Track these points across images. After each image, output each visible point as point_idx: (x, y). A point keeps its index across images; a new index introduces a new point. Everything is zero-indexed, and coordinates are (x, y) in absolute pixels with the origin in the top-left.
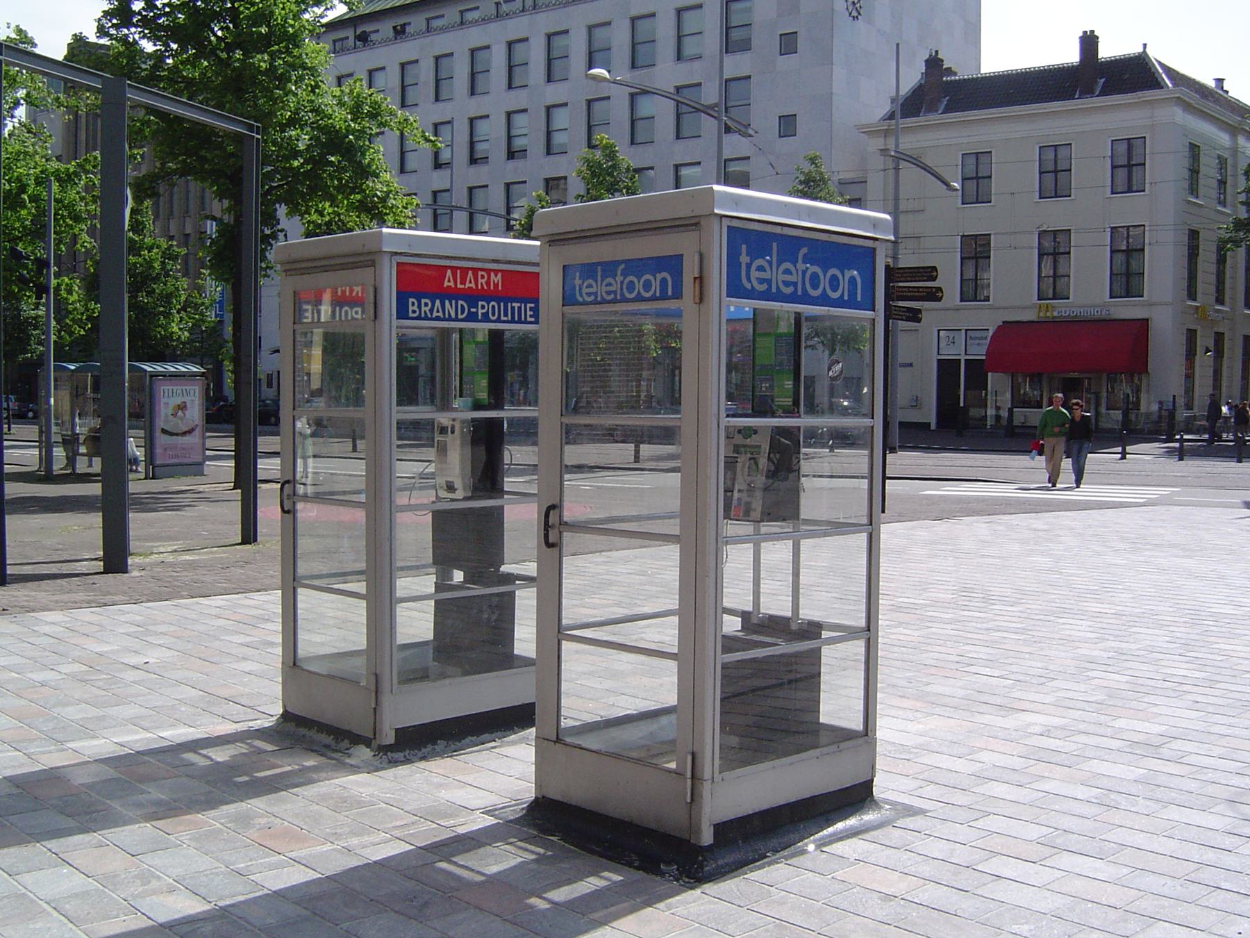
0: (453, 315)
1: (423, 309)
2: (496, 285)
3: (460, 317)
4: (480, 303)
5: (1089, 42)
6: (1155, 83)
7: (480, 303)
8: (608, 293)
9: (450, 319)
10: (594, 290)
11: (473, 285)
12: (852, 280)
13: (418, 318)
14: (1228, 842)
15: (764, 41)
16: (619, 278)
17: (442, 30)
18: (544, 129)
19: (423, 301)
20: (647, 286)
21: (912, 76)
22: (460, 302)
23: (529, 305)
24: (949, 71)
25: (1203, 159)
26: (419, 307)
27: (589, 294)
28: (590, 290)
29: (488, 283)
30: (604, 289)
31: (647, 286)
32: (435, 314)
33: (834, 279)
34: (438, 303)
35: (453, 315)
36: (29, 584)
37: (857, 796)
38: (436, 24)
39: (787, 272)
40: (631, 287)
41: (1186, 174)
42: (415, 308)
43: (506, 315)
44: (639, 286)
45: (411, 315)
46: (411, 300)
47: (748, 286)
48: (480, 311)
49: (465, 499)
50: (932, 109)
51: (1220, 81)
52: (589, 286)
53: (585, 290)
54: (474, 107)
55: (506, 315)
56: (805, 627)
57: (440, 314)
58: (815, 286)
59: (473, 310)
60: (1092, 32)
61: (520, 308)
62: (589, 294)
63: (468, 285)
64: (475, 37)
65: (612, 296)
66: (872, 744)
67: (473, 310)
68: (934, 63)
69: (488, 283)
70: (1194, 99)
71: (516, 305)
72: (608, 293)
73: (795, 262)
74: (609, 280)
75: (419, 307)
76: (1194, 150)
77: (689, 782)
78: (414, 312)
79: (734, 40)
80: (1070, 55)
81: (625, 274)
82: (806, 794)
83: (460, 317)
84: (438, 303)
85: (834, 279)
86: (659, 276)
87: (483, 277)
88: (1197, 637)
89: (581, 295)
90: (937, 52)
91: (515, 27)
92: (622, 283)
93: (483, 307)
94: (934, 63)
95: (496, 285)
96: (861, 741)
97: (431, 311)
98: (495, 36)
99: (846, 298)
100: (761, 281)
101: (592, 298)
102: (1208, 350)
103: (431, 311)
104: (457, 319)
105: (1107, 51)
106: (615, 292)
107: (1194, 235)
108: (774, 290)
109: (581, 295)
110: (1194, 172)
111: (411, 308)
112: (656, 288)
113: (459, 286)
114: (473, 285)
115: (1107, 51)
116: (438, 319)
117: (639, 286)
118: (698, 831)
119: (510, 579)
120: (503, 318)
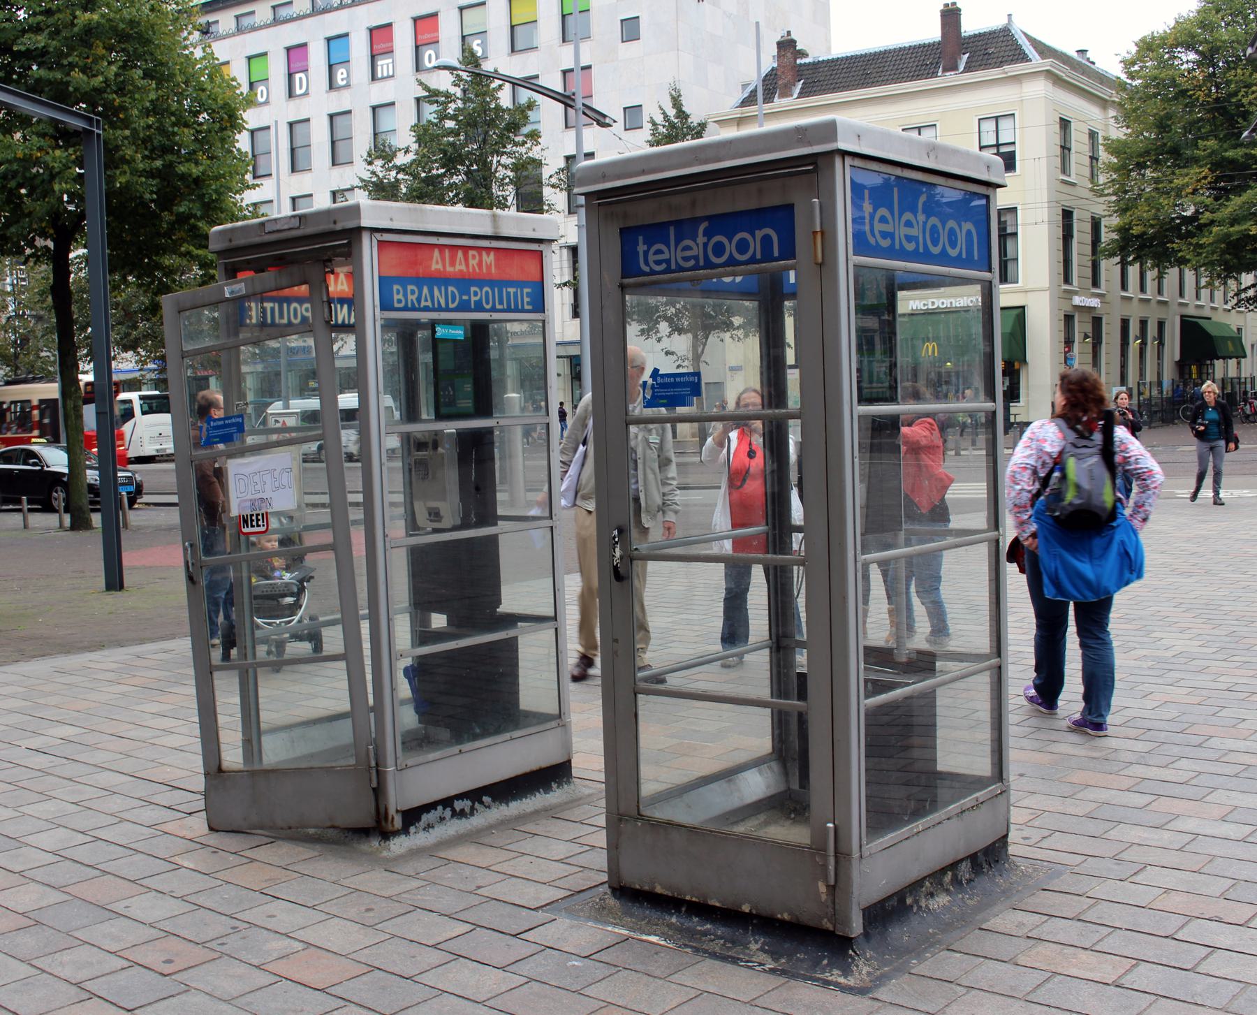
0: (443, 305)
1: (410, 297)
2: (489, 267)
3: (451, 306)
4: (473, 289)
5: (951, 16)
6: (1022, 57)
7: (473, 289)
8: (686, 259)
9: (440, 309)
10: (666, 256)
11: (463, 267)
12: (969, 233)
13: (405, 309)
14: (1092, 827)
15: (604, 25)
16: (701, 239)
17: (254, 29)
18: (371, 131)
19: (410, 287)
20: (743, 246)
21: (769, 61)
22: (450, 289)
23: (526, 290)
24: (803, 54)
25: (1074, 135)
26: (405, 296)
27: (658, 263)
28: (688, 253)
29: (480, 264)
30: (680, 254)
31: (743, 246)
32: (423, 304)
33: (952, 232)
34: (425, 290)
35: (443, 305)
36: (299, 719)
37: (990, 857)
38: (246, 22)
39: (909, 224)
40: (719, 250)
41: (1058, 151)
42: (400, 297)
43: (501, 303)
44: (730, 248)
45: (396, 305)
46: (396, 287)
47: (647, 269)
48: (473, 299)
49: (455, 528)
50: (786, 93)
51: (1082, 52)
52: (659, 252)
53: (651, 258)
54: (294, 111)
55: (501, 303)
56: (914, 656)
57: (429, 304)
58: (935, 242)
59: (465, 297)
60: (954, 4)
61: (515, 294)
62: (658, 263)
63: (458, 267)
64: (291, 34)
65: (692, 263)
66: (565, 726)
67: (465, 297)
68: (787, 46)
69: (480, 264)
70: (1064, 72)
71: (512, 290)
72: (686, 259)
73: (915, 213)
74: (688, 242)
75: (405, 296)
76: (1065, 124)
77: (832, 860)
78: (399, 301)
79: (571, 26)
80: (932, 32)
81: (709, 234)
82: (513, 775)
83: (451, 306)
84: (425, 290)
85: (952, 232)
86: (759, 234)
87: (474, 257)
88: (1133, 633)
89: (647, 263)
90: (789, 33)
91: (335, 23)
92: (705, 245)
93: (476, 294)
94: (787, 46)
95: (489, 267)
96: (553, 724)
97: (419, 300)
98: (313, 33)
99: (964, 256)
100: (885, 235)
101: (664, 266)
102: (1086, 336)
103: (419, 300)
104: (448, 310)
105: (970, 25)
106: (696, 258)
107: (1067, 215)
108: (897, 247)
109: (647, 263)
110: (1065, 149)
111: (396, 297)
112: (755, 247)
113: (449, 269)
114: (463, 267)
115: (970, 25)
116: (426, 309)
117: (730, 248)
118: (847, 922)
119: (512, 620)
120: (498, 307)
